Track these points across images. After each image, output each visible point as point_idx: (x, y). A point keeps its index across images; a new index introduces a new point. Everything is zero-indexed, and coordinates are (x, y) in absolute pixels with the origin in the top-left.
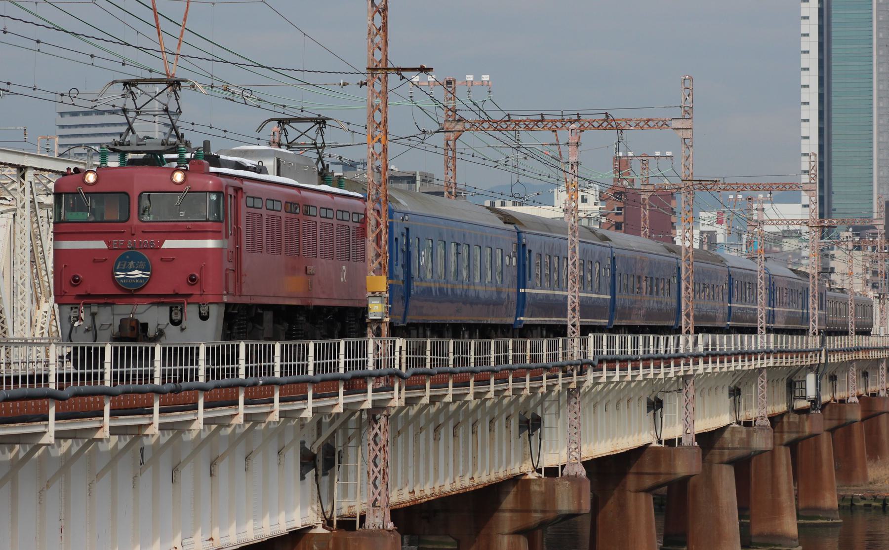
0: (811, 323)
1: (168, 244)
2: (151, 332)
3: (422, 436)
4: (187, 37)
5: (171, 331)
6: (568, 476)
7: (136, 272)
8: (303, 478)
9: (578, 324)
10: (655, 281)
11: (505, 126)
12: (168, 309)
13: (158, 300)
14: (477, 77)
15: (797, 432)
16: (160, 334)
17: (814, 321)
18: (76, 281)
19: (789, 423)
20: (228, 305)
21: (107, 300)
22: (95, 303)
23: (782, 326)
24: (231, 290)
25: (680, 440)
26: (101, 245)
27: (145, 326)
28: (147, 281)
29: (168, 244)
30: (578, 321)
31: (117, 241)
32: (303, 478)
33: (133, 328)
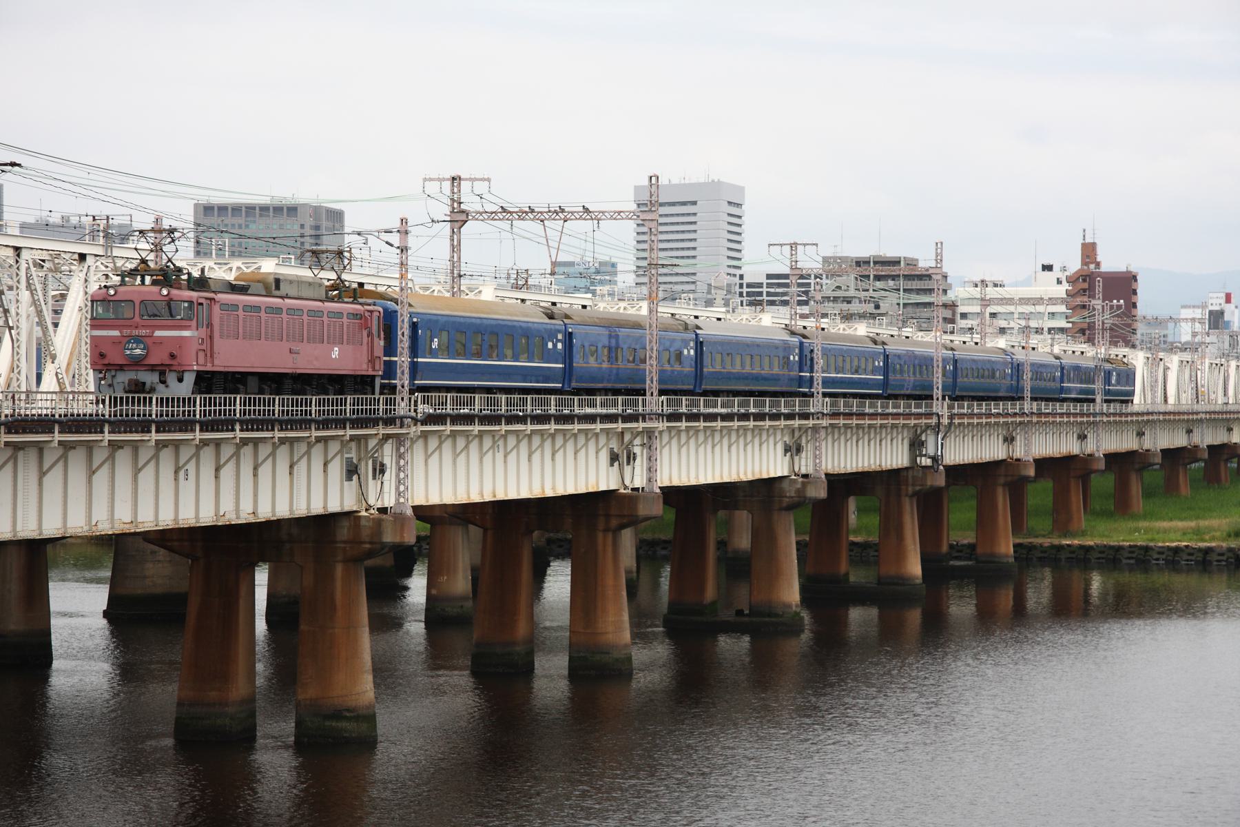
0: (935, 390)
1: (158, 333)
2: (148, 387)
3: (957, 438)
4: (584, 238)
5: (161, 387)
6: (395, 513)
7: (138, 350)
8: (785, 455)
9: (820, 393)
10: (918, 368)
11: (547, 217)
12: (158, 373)
13: (152, 368)
14: (1118, 301)
15: (922, 485)
16: (152, 390)
17: (938, 388)
18: (102, 355)
19: (913, 477)
20: (198, 372)
21: (121, 368)
22: (1117, 400)
23: (908, 392)
24: (200, 362)
25: (643, 488)
26: (116, 333)
27: (144, 384)
28: (146, 356)
29: (158, 333)
30: (821, 390)
31: (127, 332)
32: (785, 455)
33: (136, 385)
